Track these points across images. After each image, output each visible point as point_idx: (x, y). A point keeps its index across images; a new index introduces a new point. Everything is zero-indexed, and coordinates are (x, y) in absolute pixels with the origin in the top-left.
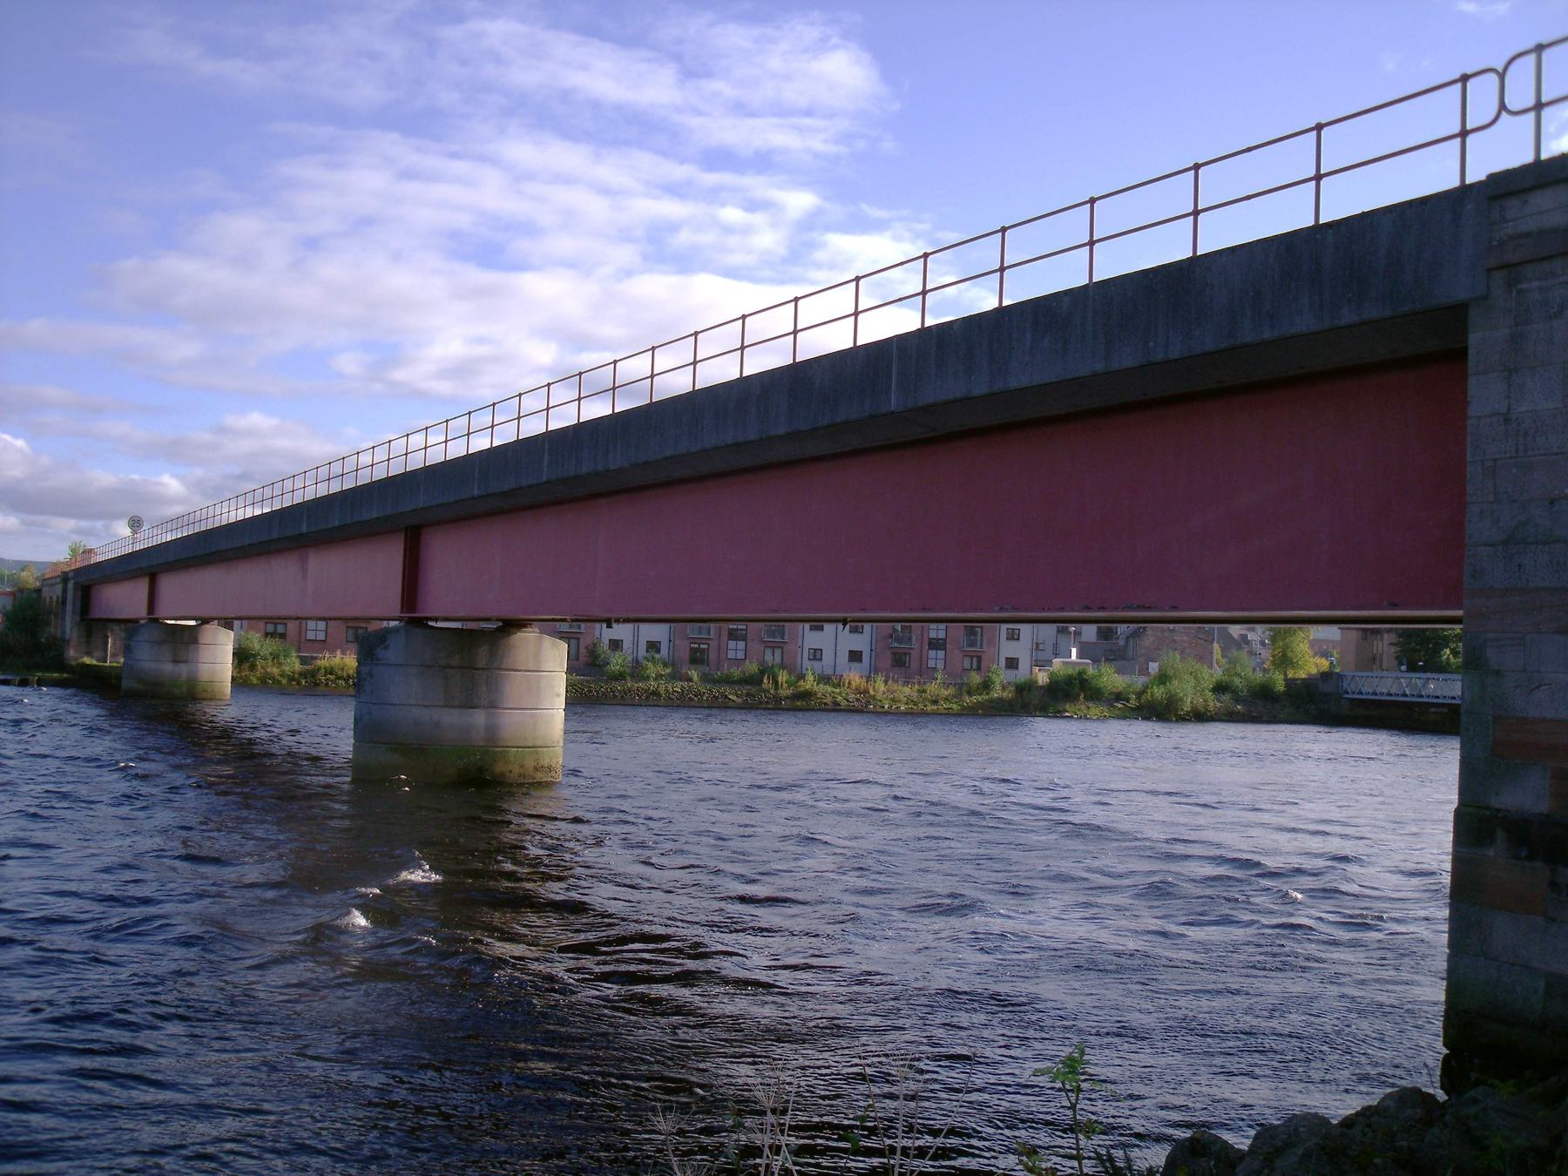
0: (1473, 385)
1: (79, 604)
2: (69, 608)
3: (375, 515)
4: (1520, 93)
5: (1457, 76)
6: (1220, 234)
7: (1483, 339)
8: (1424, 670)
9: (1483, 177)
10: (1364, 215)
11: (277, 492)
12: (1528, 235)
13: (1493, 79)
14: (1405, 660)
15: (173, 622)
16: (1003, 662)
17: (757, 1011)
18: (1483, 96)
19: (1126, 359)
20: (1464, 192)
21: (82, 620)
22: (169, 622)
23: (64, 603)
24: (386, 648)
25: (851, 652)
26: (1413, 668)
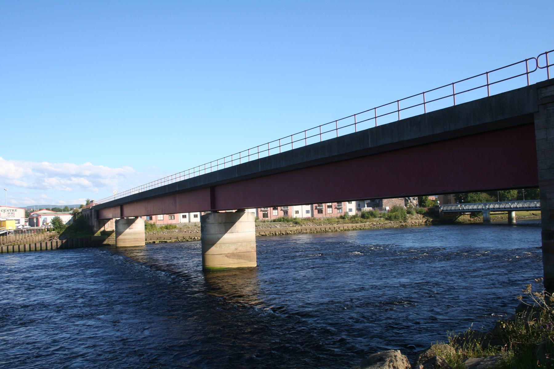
0: (537, 133)
1: (96, 215)
2: (93, 217)
3: (202, 184)
4: (542, 62)
5: (422, 92)
6: (461, 100)
7: (538, 122)
8: (464, 203)
9: (535, 83)
10: (502, 93)
11: (138, 189)
12: (548, 96)
13: (534, 60)
14: (458, 201)
15: (224, 211)
16: (294, 212)
17: (442, 317)
18: (532, 65)
19: (438, 131)
20: (529, 88)
21: (97, 220)
22: (130, 218)
23: (91, 215)
24: (209, 219)
25: (298, 211)
26: (461, 202)
